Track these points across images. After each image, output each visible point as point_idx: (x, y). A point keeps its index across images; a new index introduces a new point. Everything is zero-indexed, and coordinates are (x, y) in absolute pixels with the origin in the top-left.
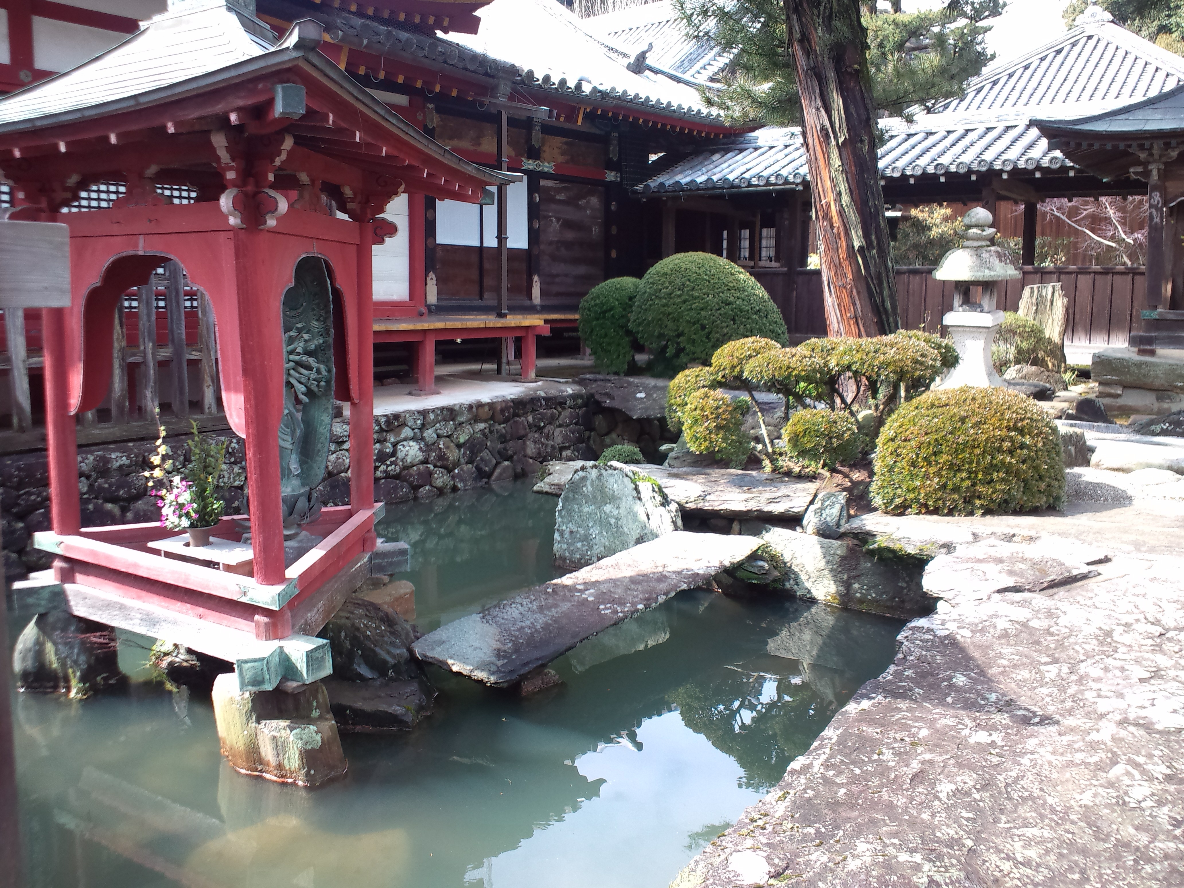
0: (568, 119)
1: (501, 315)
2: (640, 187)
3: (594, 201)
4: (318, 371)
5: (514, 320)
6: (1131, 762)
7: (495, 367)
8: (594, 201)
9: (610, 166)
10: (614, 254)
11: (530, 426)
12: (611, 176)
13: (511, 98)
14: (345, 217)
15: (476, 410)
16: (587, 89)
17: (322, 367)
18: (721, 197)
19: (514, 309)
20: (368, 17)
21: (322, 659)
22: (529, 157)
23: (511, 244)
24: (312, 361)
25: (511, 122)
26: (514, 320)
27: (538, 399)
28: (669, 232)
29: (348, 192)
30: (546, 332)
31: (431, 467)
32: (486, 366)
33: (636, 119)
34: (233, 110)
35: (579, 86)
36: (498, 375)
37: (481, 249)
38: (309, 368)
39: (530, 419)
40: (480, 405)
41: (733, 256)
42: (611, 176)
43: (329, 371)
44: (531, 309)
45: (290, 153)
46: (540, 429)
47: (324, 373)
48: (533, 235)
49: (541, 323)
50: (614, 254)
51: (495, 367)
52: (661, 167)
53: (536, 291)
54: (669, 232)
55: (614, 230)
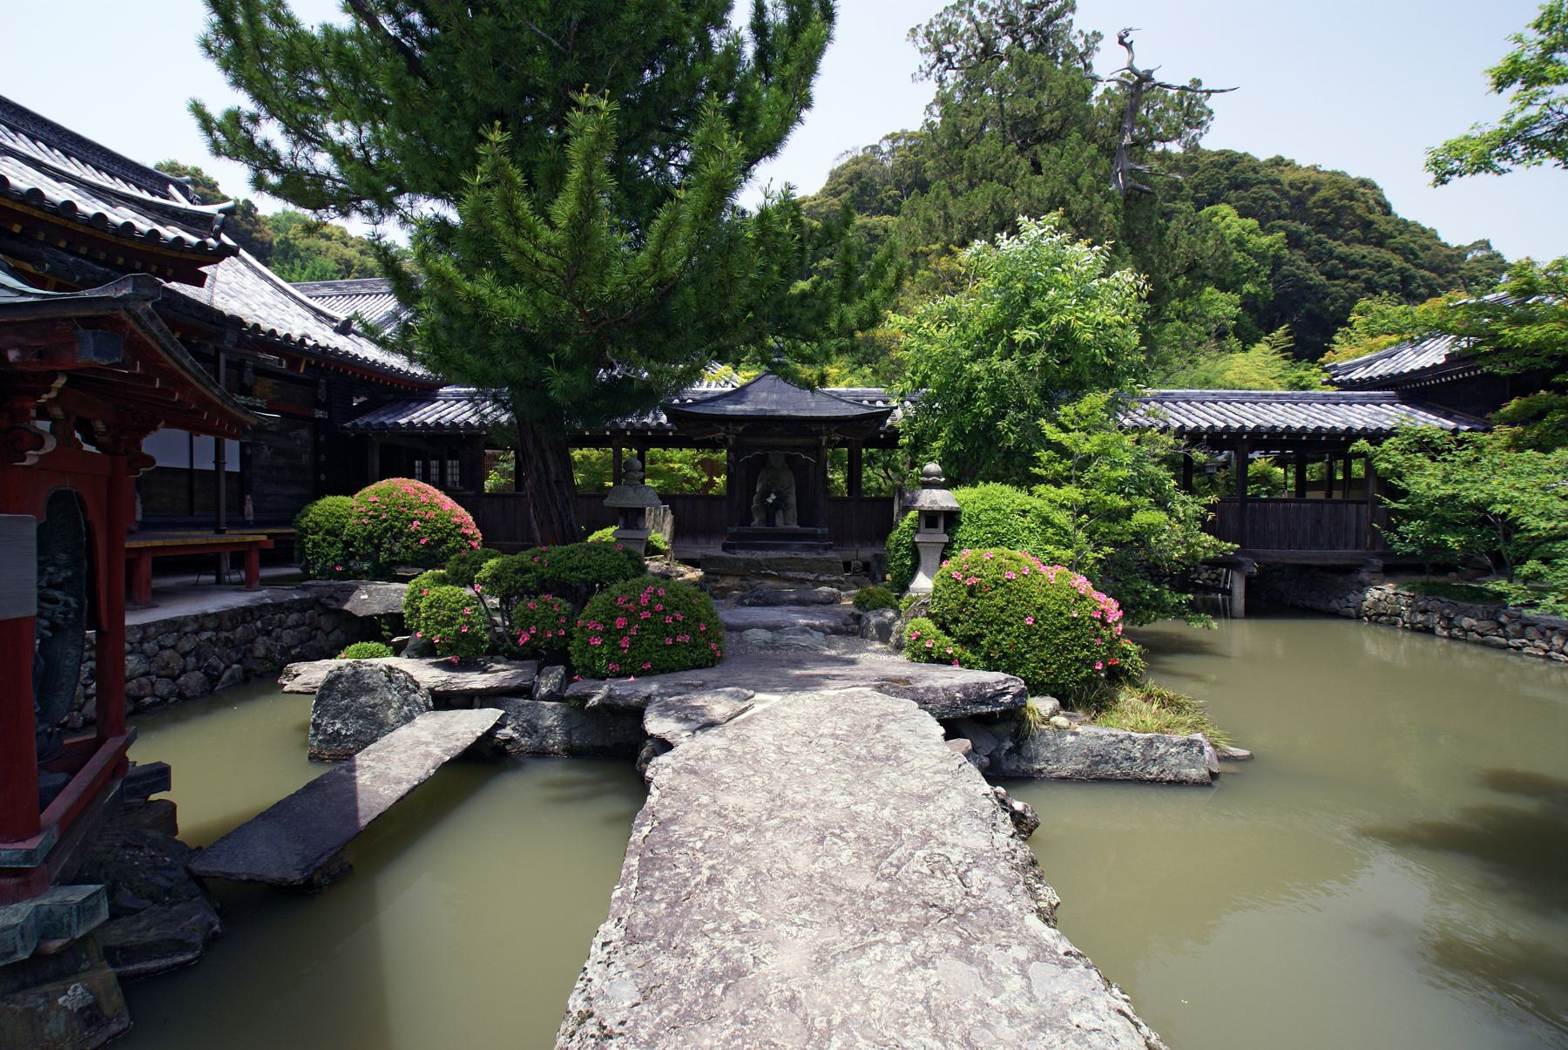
0: (290, 366)
1: (220, 532)
2: (348, 425)
3: (304, 433)
4: (67, 604)
5: (233, 536)
6: (833, 834)
7: (213, 578)
8: (304, 433)
9: (318, 405)
10: (323, 477)
11: (258, 631)
12: (320, 414)
13: (238, 345)
14: (93, 449)
15: (201, 621)
16: (310, 343)
17: (71, 600)
18: (420, 436)
19: (233, 525)
20: (82, 256)
21: (97, 906)
22: (241, 393)
23: (228, 468)
24: (57, 594)
25: (228, 364)
26: (233, 536)
27: (266, 605)
28: (375, 463)
29: (100, 426)
30: (271, 545)
31: (154, 678)
32: (203, 578)
33: (346, 371)
34: (13, 347)
35: (302, 341)
36: (221, 585)
37: (191, 472)
38: (56, 602)
39: (259, 624)
40: (206, 615)
41: (426, 479)
42: (320, 414)
43: (80, 603)
44: (245, 525)
45: (61, 391)
46: (268, 633)
47: (74, 605)
48: (244, 459)
49: (264, 538)
50: (323, 477)
51: (213, 578)
52: (363, 410)
53: (249, 507)
54: (375, 463)
55: (323, 458)
